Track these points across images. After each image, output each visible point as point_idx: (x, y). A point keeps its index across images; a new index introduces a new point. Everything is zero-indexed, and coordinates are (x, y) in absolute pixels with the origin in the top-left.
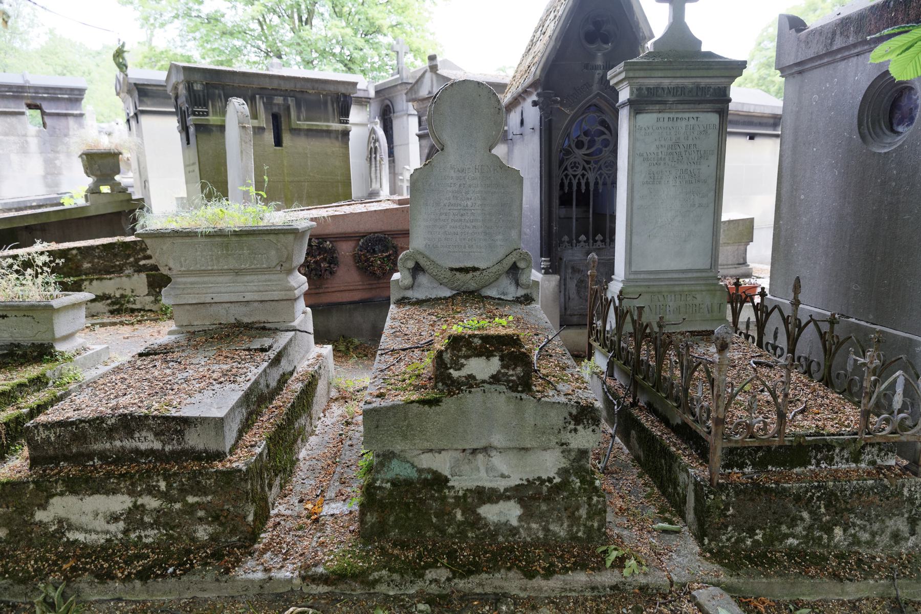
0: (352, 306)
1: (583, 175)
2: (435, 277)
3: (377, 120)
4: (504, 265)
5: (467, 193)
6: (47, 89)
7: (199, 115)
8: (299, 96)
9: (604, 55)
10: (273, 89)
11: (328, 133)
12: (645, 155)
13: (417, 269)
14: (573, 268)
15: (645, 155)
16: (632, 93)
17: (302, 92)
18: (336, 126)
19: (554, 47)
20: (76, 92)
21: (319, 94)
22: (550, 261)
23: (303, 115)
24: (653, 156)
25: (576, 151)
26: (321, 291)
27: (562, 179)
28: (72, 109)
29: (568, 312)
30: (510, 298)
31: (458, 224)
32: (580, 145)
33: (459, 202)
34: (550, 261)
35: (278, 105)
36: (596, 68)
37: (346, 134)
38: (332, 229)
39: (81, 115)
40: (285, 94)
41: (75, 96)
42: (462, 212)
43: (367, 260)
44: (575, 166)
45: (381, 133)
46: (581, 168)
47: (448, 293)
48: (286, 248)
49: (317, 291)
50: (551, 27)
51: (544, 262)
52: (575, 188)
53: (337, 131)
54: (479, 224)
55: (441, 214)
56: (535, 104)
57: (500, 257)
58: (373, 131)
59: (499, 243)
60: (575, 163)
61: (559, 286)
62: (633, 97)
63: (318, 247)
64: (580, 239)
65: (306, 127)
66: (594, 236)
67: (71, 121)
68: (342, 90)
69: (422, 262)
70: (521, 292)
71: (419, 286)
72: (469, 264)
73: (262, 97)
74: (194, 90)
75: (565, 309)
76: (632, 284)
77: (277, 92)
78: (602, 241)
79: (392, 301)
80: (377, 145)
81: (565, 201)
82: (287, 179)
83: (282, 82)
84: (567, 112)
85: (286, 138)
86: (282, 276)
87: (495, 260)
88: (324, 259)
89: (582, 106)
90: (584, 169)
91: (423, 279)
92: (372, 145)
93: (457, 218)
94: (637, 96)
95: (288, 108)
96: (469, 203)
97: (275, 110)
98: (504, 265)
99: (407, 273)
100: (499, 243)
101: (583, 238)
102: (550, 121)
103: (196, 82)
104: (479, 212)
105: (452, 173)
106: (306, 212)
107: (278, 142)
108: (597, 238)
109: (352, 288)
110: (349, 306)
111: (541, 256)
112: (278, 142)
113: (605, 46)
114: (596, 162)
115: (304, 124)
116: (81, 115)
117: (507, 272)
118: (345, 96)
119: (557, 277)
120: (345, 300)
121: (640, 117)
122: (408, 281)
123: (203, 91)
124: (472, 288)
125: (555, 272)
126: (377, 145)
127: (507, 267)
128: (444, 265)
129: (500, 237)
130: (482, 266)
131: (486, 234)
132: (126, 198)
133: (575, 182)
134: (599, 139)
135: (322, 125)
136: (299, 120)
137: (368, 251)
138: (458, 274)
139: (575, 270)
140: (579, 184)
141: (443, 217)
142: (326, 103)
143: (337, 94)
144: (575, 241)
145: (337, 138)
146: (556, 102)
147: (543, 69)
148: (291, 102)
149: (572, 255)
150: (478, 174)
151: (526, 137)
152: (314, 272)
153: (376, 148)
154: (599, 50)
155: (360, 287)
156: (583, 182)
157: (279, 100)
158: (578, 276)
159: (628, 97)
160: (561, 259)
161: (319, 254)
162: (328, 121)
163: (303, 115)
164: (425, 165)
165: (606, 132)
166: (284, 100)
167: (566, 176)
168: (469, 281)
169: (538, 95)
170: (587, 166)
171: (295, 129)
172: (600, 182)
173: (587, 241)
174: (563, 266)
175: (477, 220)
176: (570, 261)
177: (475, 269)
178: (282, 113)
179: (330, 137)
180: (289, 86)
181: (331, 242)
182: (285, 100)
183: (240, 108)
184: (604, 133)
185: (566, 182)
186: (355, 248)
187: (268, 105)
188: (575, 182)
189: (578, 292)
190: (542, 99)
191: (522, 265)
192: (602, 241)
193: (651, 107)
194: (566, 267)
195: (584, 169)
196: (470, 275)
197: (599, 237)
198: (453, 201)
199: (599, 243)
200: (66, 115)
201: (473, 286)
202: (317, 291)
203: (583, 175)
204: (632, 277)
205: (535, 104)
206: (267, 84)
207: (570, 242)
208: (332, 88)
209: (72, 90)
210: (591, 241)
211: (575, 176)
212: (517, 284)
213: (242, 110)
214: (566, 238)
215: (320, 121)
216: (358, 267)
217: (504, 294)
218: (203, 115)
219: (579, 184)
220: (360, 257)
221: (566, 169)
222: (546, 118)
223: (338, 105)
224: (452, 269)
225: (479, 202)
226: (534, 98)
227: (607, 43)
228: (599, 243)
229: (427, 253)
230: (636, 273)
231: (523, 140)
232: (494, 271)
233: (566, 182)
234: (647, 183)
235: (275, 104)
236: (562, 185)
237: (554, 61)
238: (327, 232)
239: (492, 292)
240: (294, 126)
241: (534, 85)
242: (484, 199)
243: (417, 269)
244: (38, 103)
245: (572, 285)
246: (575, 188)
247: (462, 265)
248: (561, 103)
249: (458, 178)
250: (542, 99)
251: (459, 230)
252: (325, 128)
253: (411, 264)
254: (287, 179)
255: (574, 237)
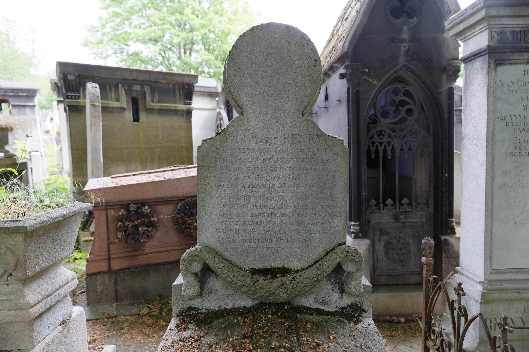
0: (170, 266)
1: (389, 143)
2: (230, 284)
3: (222, 106)
4: (325, 268)
5: (273, 170)
6: (12, 90)
7: (72, 98)
8: (153, 84)
9: (410, 29)
10: (132, 80)
11: (175, 112)
12: (508, 118)
13: (206, 273)
14: (381, 230)
15: (508, 118)
16: (491, 38)
17: (156, 82)
18: (181, 107)
19: (361, 21)
20: (32, 92)
21: (169, 83)
22: (359, 225)
23: (156, 98)
24: (519, 119)
25: (382, 120)
26: (139, 253)
27: (369, 147)
28: (28, 102)
29: (377, 273)
30: (331, 308)
31: (262, 211)
32: (385, 114)
33: (262, 182)
34: (359, 225)
35: (137, 91)
36: (402, 41)
37: (189, 113)
38: (151, 194)
39: (34, 106)
40: (142, 83)
41: (31, 94)
42: (267, 195)
43: (185, 222)
44: (381, 134)
45: (224, 114)
46: (386, 136)
47: (248, 303)
48: (13, 252)
49: (135, 253)
50: (345, 29)
51: (354, 226)
52: (381, 154)
53: (182, 111)
54: (290, 211)
55: (239, 198)
56: (342, 76)
57: (320, 252)
58: (219, 113)
59: (316, 236)
60: (381, 131)
61: (369, 250)
62: (493, 44)
63: (136, 212)
64: (387, 202)
65: (158, 108)
66: (400, 200)
67: (27, 110)
68: (187, 80)
69: (213, 263)
70: (346, 301)
71: (209, 293)
72: (277, 264)
73: (123, 86)
74: (68, 80)
75: (374, 270)
76: (494, 287)
77: (136, 81)
78: (408, 204)
79: (174, 314)
80: (222, 122)
81: (372, 164)
82: (142, 146)
83: (139, 75)
84: (375, 82)
85: (143, 116)
86: (16, 287)
87: (312, 259)
88: (142, 224)
89: (388, 78)
90: (390, 136)
91: (214, 284)
92: (219, 122)
93: (260, 203)
94: (498, 42)
95: (144, 94)
96: (277, 184)
97: (134, 95)
98: (325, 268)
99: (191, 278)
100: (316, 236)
101: (389, 201)
102: (358, 92)
103: (70, 74)
104: (290, 195)
105: (253, 145)
106: (139, 176)
107: (136, 119)
108: (403, 202)
109: (169, 248)
110: (166, 266)
111: (351, 220)
112: (136, 119)
113: (411, 21)
114: (401, 130)
115: (157, 105)
116: (34, 106)
117: (329, 277)
118: (189, 85)
119: (367, 241)
120: (162, 261)
121: (501, 69)
122: (193, 289)
123: (75, 80)
124: (280, 300)
125: (365, 236)
126: (222, 122)
127: (329, 270)
128: (243, 266)
129: (318, 228)
130: (294, 265)
131: (299, 223)
132: (12, 162)
133: (381, 150)
134: (403, 109)
135: (171, 106)
136: (153, 102)
137: (186, 214)
138: (261, 278)
139: (383, 232)
140: (385, 151)
141: (242, 202)
142: (174, 90)
143: (183, 83)
144: (382, 205)
145: (182, 115)
146: (364, 73)
147: (351, 42)
148: (147, 89)
149: (383, 218)
150: (287, 146)
151: (330, 110)
152: (131, 236)
153: (221, 124)
154: (404, 24)
155: (177, 248)
156: (389, 149)
157: (137, 88)
158: (385, 238)
159: (487, 43)
160: (369, 222)
161: (138, 219)
162: (176, 103)
163: (156, 98)
164: (218, 134)
165: (411, 102)
166: (141, 87)
167: (373, 143)
168: (275, 290)
169: (346, 68)
170: (393, 134)
171: (150, 109)
172: (406, 149)
173: (394, 205)
174: (371, 229)
175: (286, 206)
176: (378, 223)
177: (285, 271)
178: (139, 97)
179: (177, 115)
180: (145, 77)
181: (149, 206)
182: (142, 87)
183: (93, 90)
184: (408, 103)
185: (373, 150)
186: (174, 210)
187: (128, 91)
188: (381, 150)
189: (386, 253)
190: (349, 71)
191: (349, 268)
192: (408, 204)
193: (517, 56)
194: (374, 230)
195: (390, 136)
196: (277, 282)
197: (405, 201)
198: (254, 181)
199: (405, 206)
200: (24, 106)
201: (282, 296)
202: (135, 253)
203: (389, 143)
204: (494, 277)
205: (342, 76)
206: (127, 76)
207: (377, 205)
208: (179, 79)
209: (29, 91)
210: (398, 205)
211: (381, 144)
212: (342, 290)
213: (94, 92)
214: (373, 202)
215: (169, 103)
216: (176, 228)
217: (324, 303)
218: (75, 98)
219: (385, 151)
220: (178, 219)
221: (372, 137)
222: (353, 89)
223: (184, 92)
224: (254, 272)
225: (289, 182)
226: (342, 71)
227: (410, 17)
228: (405, 206)
229: (220, 249)
230: (498, 271)
231: (328, 112)
232: (311, 276)
233: (373, 150)
234: (512, 154)
235: (134, 91)
236: (369, 152)
237: (361, 35)
238: (146, 197)
239: (309, 302)
240: (148, 107)
241: (341, 60)
242: (297, 178)
243: (206, 273)
244: (6, 98)
245: (380, 247)
246: (381, 154)
247: (267, 265)
248: (368, 74)
249: (261, 151)
250: (349, 71)
251: (263, 219)
252: (165, 108)
253: (197, 267)
254: (142, 146)
255: (381, 201)
